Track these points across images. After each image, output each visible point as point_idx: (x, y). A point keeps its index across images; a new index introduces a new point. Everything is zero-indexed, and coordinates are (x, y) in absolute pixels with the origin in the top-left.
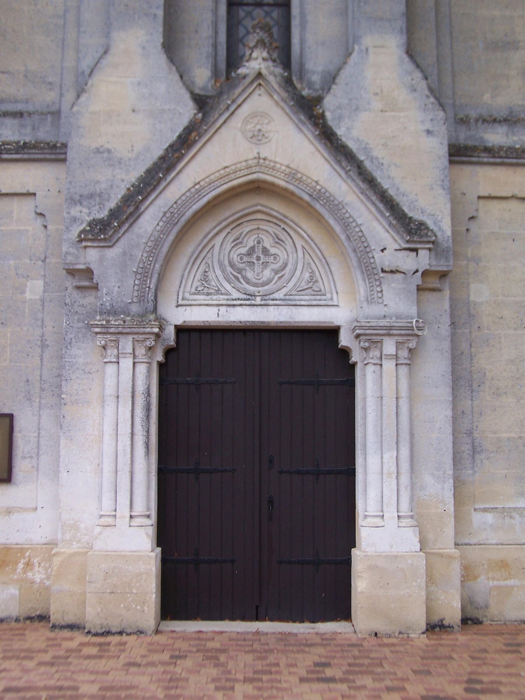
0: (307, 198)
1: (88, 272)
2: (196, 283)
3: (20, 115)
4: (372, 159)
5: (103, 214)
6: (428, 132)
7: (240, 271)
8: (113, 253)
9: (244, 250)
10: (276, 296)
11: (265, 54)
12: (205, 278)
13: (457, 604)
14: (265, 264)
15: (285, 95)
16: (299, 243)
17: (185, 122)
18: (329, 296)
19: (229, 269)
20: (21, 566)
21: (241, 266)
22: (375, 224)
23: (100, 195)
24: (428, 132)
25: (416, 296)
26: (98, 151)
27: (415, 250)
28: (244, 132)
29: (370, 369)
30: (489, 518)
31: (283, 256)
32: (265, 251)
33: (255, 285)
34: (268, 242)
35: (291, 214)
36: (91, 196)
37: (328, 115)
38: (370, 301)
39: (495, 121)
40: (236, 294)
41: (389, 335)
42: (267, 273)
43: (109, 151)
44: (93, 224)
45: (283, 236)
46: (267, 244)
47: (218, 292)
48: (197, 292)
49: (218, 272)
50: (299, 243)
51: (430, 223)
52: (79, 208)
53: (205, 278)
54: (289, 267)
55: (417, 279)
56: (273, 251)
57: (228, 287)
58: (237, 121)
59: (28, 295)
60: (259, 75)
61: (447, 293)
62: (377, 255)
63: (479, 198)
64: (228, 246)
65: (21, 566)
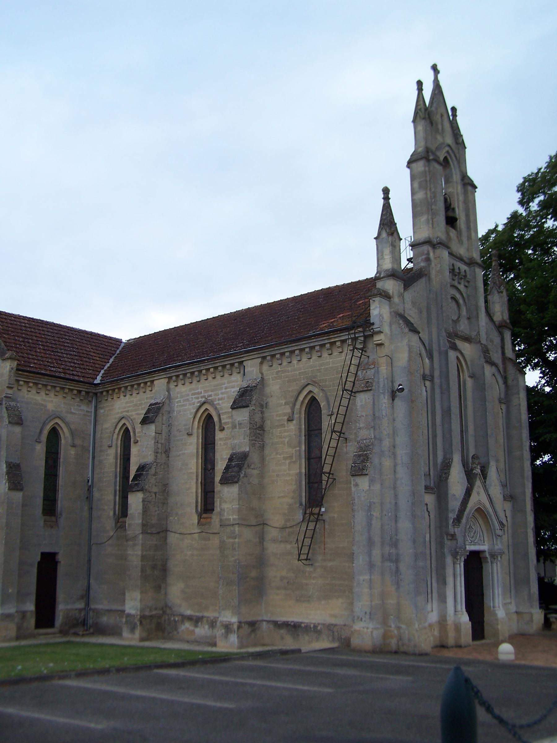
8: (459, 529)
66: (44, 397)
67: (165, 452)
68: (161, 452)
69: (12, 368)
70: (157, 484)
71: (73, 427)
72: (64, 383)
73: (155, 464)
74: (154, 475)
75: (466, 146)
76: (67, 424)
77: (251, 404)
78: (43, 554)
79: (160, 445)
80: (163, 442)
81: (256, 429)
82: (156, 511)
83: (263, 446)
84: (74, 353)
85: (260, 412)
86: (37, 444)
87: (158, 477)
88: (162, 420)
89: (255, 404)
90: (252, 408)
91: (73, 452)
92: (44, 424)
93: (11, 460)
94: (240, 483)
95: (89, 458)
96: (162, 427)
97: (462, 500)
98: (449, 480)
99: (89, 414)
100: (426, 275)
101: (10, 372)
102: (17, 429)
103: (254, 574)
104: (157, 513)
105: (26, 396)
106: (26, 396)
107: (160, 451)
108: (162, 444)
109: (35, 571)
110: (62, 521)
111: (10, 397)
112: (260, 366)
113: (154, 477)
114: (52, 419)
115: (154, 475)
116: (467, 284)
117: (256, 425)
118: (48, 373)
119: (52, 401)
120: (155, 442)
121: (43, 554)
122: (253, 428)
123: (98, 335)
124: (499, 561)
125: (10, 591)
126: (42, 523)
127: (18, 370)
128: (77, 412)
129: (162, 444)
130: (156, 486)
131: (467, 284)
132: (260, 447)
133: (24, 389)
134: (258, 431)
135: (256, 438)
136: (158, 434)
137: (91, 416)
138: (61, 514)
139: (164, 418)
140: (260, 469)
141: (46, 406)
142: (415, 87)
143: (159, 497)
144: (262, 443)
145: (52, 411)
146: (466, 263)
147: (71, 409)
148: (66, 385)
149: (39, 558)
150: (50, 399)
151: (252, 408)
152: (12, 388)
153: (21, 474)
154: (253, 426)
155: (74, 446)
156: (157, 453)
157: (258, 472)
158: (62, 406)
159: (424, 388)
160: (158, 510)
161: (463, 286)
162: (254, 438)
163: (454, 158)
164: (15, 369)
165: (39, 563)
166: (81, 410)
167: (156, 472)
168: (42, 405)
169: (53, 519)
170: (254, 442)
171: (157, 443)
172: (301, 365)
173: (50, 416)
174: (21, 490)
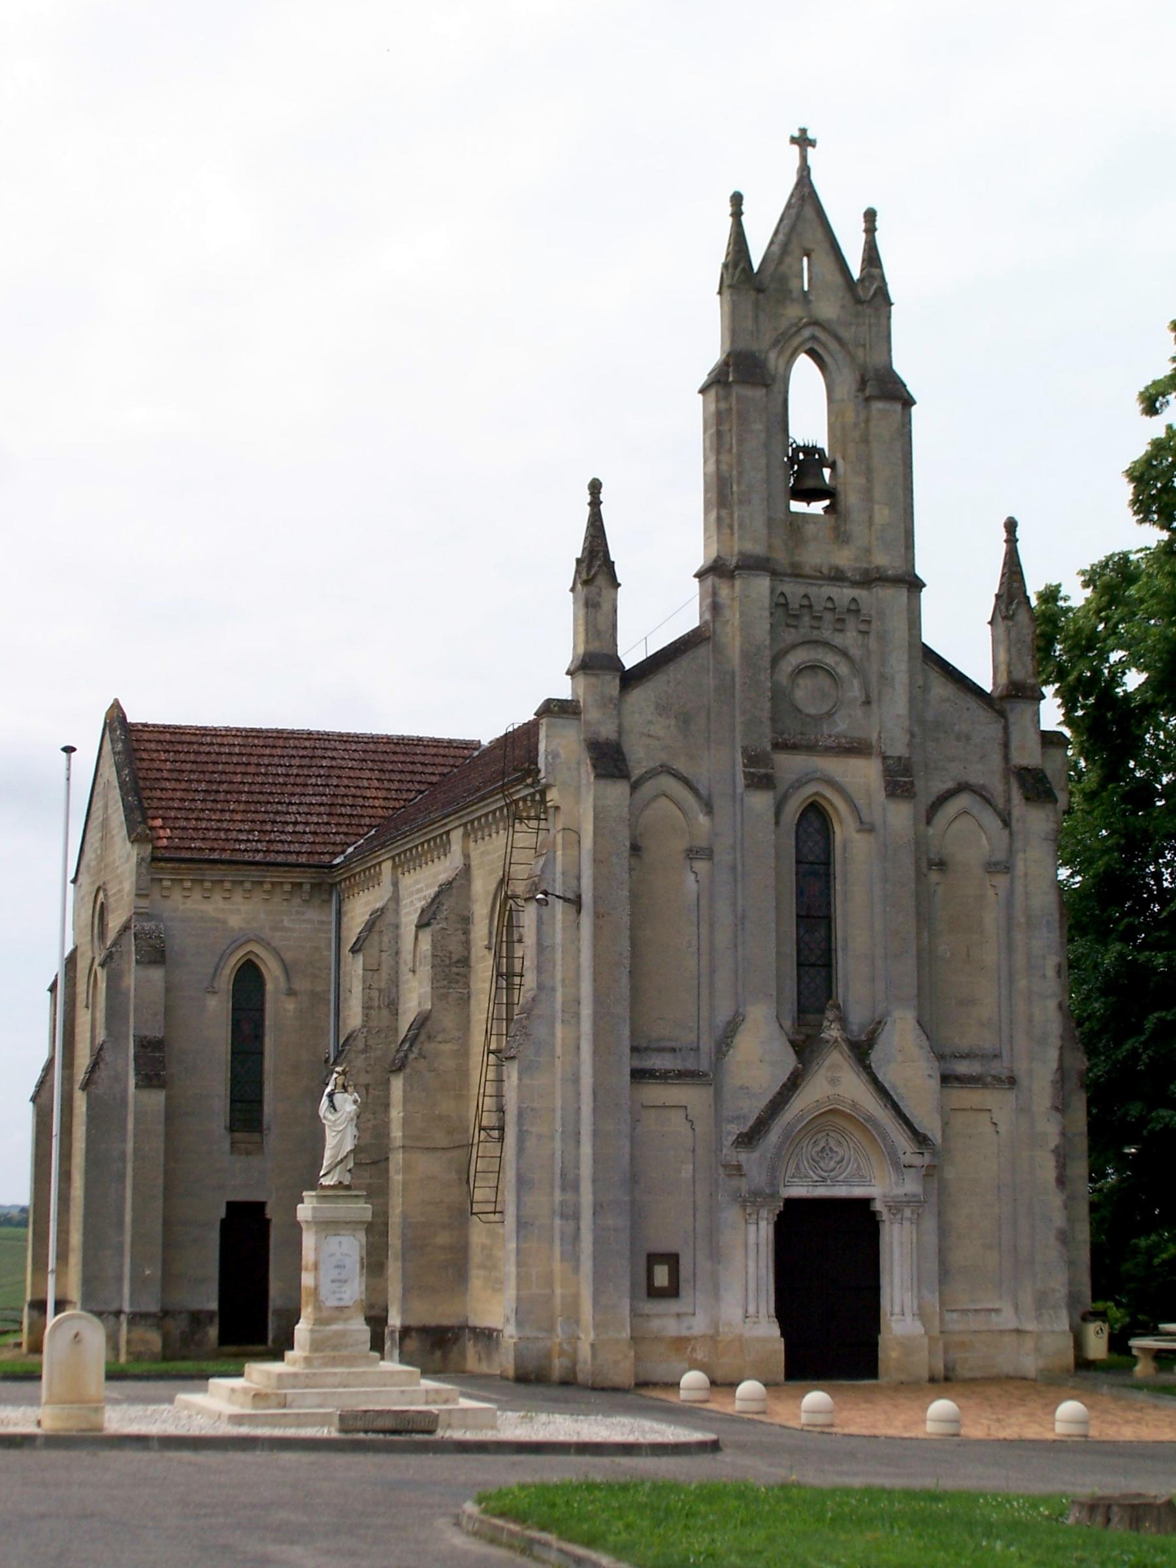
0: (862, 1120)
1: (739, 1167)
2: (793, 1171)
3: (673, 1050)
4: (897, 1095)
5: (745, 1129)
6: (930, 1076)
7: (817, 1162)
8: (755, 1155)
9: (819, 1148)
10: (839, 1179)
11: (839, 1027)
12: (798, 1168)
13: (942, 1366)
14: (831, 1158)
15: (850, 1054)
16: (851, 1145)
17: (790, 1069)
18: (868, 1179)
19: (811, 1161)
20: (689, 1350)
21: (818, 1159)
22: (900, 1137)
23: (744, 1118)
24: (930, 1076)
25: (461, 844)
26: (741, 1088)
27: (922, 1153)
28: (826, 1078)
29: (896, 1227)
30: (955, 1316)
31: (841, 1153)
32: (831, 1149)
33: (826, 1171)
34: (832, 1143)
35: (849, 1127)
36: (738, 1118)
37: (873, 1065)
38: (897, 1184)
39: (961, 1057)
40: (816, 1178)
41: (908, 1206)
42: (832, 1164)
43: (747, 1088)
44: (739, 1135)
45: (842, 1140)
46: (832, 1146)
47: (806, 1177)
48: (793, 1177)
49: (806, 1163)
50: (851, 1145)
51: (930, 1135)
52: (733, 1126)
53: (798, 1168)
54: (844, 1162)
55: (923, 1171)
56: (835, 1149)
57: (812, 1173)
58: (822, 1071)
59: (683, 1175)
60: (836, 1041)
61: (936, 1176)
62: (902, 1156)
63: (952, 1109)
64: (810, 1147)
65: (689, 1350)
66: (221, 904)
67: (388, 1006)
68: (379, 1007)
69: (143, 859)
70: (369, 1068)
71: (288, 956)
72: (258, 873)
73: (365, 1030)
74: (364, 1051)
75: (893, 300)
76: (276, 953)
77: (435, 918)
78: (231, 1206)
79: (375, 994)
80: (383, 985)
81: (449, 966)
82: (369, 1120)
83: (469, 997)
84: (324, 798)
85: (460, 932)
86: (208, 995)
87: (372, 1055)
88: (381, 942)
89: (447, 918)
90: (440, 926)
91: (290, 1005)
92: (224, 957)
93: (146, 1032)
94: (408, 1070)
95: (328, 1016)
96: (380, 957)
97: (775, 1097)
98: (726, 1059)
99: (326, 927)
100: (708, 638)
101: (139, 864)
102: (156, 974)
103: (443, 1238)
104: (370, 1124)
105: (181, 907)
106: (181, 907)
107: (376, 1004)
108: (380, 990)
109: (214, 1236)
110: (272, 1140)
111: (146, 914)
112: (463, 842)
113: (364, 1056)
114: (241, 946)
115: (364, 1051)
116: (863, 627)
117: (450, 958)
118: (226, 856)
119: (238, 910)
120: (363, 989)
121: (231, 1206)
122: (442, 963)
123: (419, 741)
124: (907, 1219)
125: (148, 1272)
126: (226, 1146)
127: (154, 859)
128: (297, 926)
129: (380, 990)
130: (367, 1072)
131: (863, 627)
132: (461, 999)
133: (177, 895)
134: (455, 970)
135: (449, 982)
136: (370, 973)
137: (330, 930)
138: (269, 1129)
139: (385, 939)
140: (460, 1041)
141: (224, 922)
142: (728, 209)
143: (377, 1093)
144: (466, 991)
145: (240, 929)
146: (855, 584)
147: (282, 921)
148: (266, 877)
149: (222, 1213)
150: (235, 907)
151: (440, 926)
152: (147, 896)
153: (163, 1057)
154: (443, 961)
155: (291, 992)
156: (370, 1008)
157: (455, 1048)
158: (262, 916)
159: (692, 877)
160: (375, 1119)
161: (855, 634)
162: (445, 982)
163: (833, 345)
164: (149, 859)
165: (224, 1223)
166: (305, 920)
167: (366, 1046)
168: (218, 920)
169: (256, 1137)
170: (445, 990)
171: (369, 988)
172: (189, 904)
173: (235, 941)
174: (162, 1086)
